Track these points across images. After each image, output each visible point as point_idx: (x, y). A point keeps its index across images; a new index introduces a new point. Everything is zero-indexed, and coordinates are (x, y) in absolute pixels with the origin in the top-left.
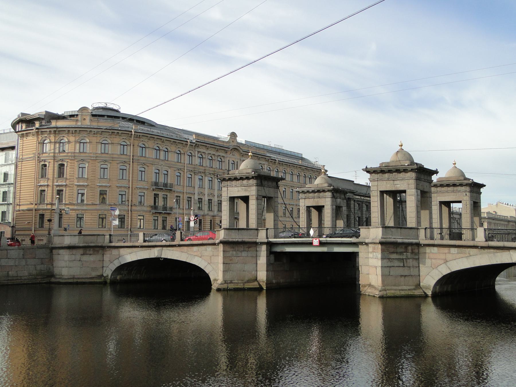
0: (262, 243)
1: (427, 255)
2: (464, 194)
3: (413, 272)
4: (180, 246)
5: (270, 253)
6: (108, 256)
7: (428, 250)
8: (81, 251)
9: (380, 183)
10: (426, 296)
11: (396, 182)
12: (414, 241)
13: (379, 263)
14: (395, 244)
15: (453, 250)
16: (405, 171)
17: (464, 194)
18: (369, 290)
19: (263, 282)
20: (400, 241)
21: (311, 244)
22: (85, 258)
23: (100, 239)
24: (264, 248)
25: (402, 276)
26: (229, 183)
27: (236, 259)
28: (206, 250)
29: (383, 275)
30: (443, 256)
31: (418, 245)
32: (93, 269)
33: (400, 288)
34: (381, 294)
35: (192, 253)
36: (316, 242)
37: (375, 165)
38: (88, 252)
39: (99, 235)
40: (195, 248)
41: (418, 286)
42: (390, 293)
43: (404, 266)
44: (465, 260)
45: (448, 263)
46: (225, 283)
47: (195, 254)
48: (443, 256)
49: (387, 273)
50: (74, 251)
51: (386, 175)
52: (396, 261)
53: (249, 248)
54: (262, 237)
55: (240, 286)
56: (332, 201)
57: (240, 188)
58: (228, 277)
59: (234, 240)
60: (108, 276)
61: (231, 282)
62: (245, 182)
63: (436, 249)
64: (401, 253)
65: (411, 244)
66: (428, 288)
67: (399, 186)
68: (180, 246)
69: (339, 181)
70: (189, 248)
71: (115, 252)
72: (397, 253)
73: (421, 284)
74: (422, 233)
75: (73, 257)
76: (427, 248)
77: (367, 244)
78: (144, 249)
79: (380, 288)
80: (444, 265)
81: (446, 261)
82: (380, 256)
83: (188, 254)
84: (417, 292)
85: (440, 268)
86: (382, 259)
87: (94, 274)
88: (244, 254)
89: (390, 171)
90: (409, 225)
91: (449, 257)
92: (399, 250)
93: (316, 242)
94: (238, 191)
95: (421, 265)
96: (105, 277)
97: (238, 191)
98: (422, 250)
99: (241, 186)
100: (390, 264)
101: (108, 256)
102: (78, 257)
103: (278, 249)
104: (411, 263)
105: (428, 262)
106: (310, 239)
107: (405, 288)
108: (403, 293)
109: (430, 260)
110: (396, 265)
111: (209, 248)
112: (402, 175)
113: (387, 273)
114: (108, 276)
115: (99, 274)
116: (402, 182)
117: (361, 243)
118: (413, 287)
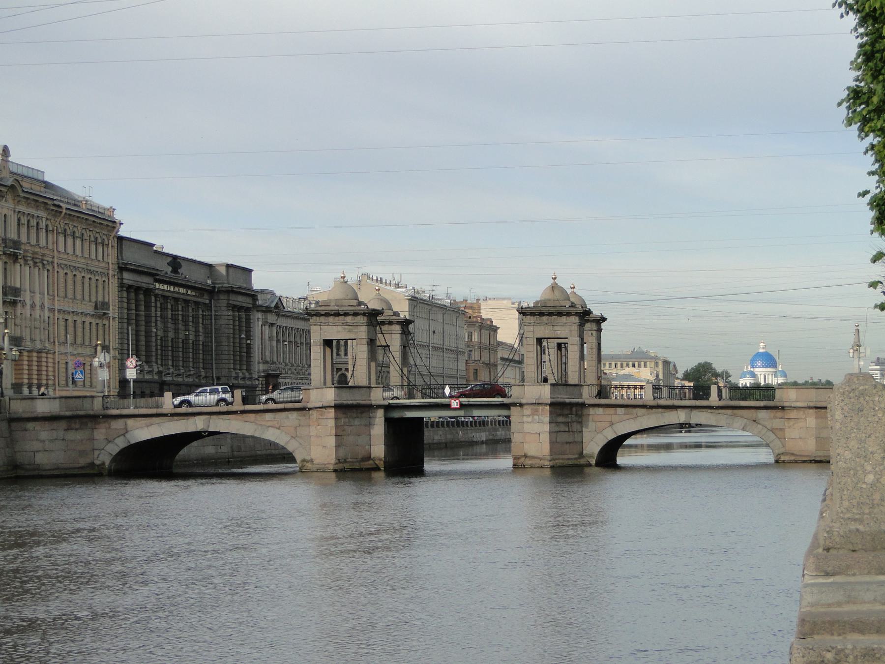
0: (379, 407)
1: (591, 418)
2: (590, 333)
3: (577, 438)
4: (243, 412)
5: (389, 421)
6: (103, 431)
7: (592, 411)
8: (63, 424)
9: (537, 328)
10: (590, 465)
11: (556, 328)
12: (580, 401)
13: (547, 428)
14: (562, 405)
15: (620, 411)
16: (568, 314)
17: (590, 333)
18: (530, 462)
19: (380, 460)
20: (567, 400)
21: (447, 407)
22: (72, 435)
23: (87, 403)
24: (380, 413)
25: (567, 443)
26: (323, 319)
27: (349, 429)
28: (288, 417)
29: (551, 443)
30: (608, 418)
31: (583, 405)
32: (82, 453)
33: (566, 457)
34: (551, 463)
35: (263, 423)
36: (455, 404)
37: (529, 302)
38: (73, 426)
39: (85, 397)
40: (268, 416)
41: (581, 455)
42: (559, 462)
43: (569, 431)
44: (632, 421)
45: (614, 426)
46: (340, 462)
47: (269, 424)
48: (608, 418)
49: (554, 440)
50: (55, 425)
51: (545, 318)
52: (562, 425)
53: (362, 413)
54: (378, 396)
55: (357, 466)
56: (402, 339)
57: (340, 328)
58: (342, 454)
59: (345, 402)
60: (103, 464)
61: (345, 461)
62: (349, 319)
63: (601, 409)
64: (566, 416)
65: (577, 404)
66: (591, 456)
67: (561, 331)
68: (243, 412)
69: (136, 245)
70: (258, 416)
71: (118, 424)
72: (563, 415)
73: (584, 452)
74: (585, 391)
75: (54, 434)
76: (591, 409)
77: (521, 405)
78: (176, 418)
79: (548, 458)
80: (610, 428)
81: (612, 424)
82: (547, 419)
83: (256, 424)
84: (582, 461)
85: (605, 432)
86: (551, 422)
87: (83, 462)
88: (357, 422)
89: (550, 314)
90: (571, 382)
91: (615, 418)
92: (566, 412)
93: (455, 404)
94: (338, 332)
95: (584, 429)
96: (98, 466)
97: (338, 332)
98: (585, 411)
99: (343, 324)
100: (557, 429)
101: (103, 431)
102: (61, 434)
103: (396, 415)
104: (576, 427)
105: (592, 425)
106: (447, 400)
107: (570, 456)
108: (570, 462)
109: (594, 424)
110: (562, 429)
111: (294, 416)
112: (564, 319)
113: (554, 440)
114: (103, 464)
115: (89, 461)
116: (563, 328)
117: (514, 405)
118: (576, 456)
